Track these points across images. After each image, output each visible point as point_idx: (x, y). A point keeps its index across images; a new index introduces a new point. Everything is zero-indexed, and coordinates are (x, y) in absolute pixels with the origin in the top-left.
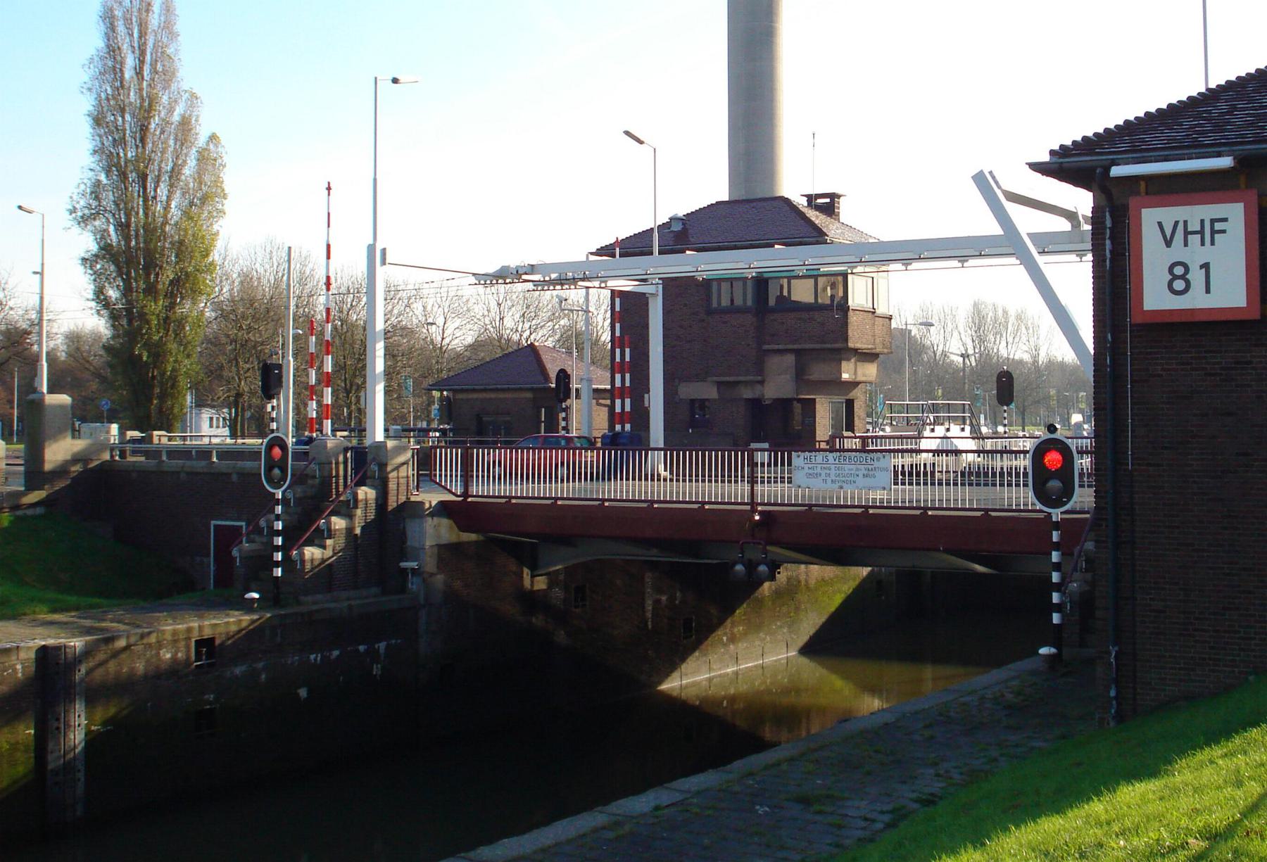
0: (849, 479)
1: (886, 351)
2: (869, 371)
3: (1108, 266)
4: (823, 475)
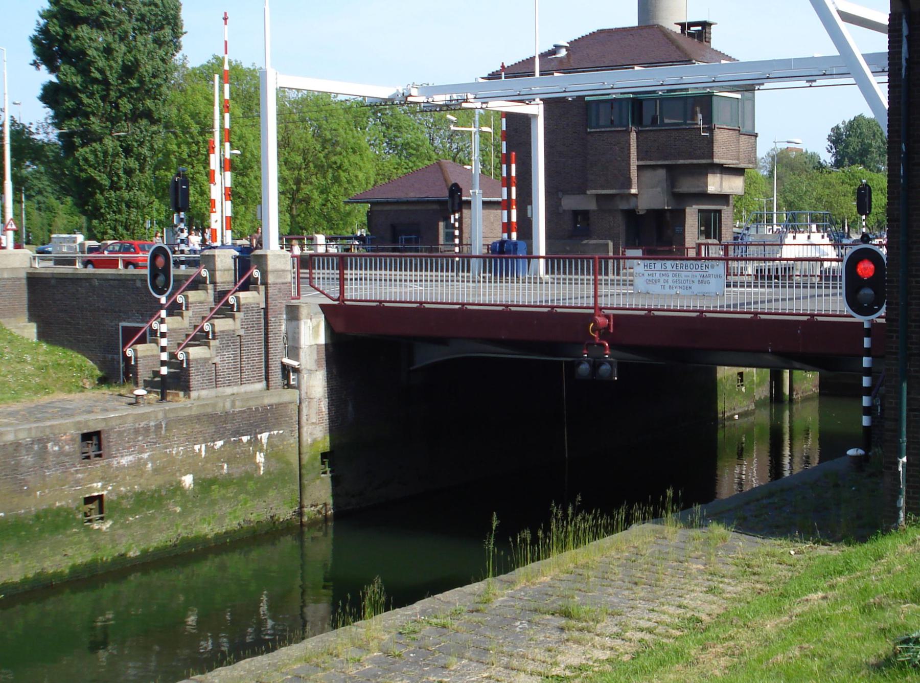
0: (685, 285)
1: (751, 166)
2: (733, 185)
3: (903, 74)
4: (662, 281)
